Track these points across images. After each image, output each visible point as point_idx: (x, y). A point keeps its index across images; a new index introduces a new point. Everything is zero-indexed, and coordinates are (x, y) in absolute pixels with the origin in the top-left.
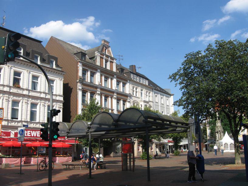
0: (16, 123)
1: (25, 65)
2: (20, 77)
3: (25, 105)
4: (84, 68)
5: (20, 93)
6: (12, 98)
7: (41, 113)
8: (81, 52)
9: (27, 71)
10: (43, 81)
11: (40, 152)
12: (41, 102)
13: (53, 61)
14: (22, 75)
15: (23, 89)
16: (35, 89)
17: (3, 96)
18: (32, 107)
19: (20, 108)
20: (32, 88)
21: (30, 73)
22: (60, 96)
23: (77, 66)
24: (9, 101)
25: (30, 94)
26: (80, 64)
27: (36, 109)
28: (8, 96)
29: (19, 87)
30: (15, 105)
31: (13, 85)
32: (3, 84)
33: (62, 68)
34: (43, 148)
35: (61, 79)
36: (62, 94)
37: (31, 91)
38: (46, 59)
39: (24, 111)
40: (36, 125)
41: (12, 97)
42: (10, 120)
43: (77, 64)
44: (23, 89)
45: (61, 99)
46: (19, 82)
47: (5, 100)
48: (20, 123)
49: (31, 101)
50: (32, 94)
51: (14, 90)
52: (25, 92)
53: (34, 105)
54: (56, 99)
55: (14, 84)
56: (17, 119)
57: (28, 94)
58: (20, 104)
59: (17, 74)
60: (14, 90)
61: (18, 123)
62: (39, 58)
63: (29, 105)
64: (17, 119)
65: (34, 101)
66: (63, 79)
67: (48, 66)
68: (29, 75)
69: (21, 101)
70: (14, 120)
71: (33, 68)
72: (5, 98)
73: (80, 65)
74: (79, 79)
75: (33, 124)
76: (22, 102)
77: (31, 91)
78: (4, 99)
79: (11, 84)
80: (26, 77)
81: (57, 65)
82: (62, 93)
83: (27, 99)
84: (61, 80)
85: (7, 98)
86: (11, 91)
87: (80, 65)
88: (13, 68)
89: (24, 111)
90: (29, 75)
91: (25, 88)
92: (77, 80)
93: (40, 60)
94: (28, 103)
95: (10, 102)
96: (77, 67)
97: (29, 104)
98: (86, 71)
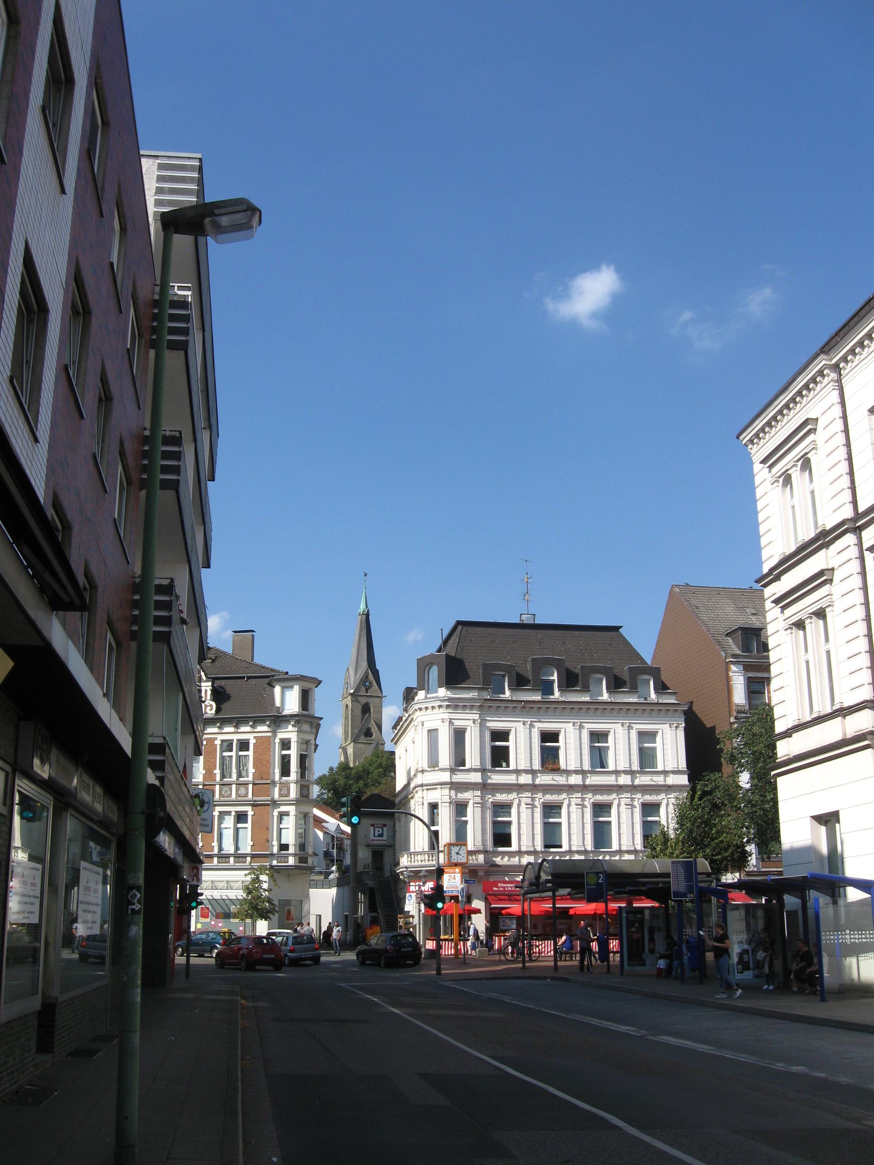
0: (506, 858)
1: (582, 711)
2: (557, 741)
3: (625, 812)
4: (751, 675)
5: (660, 783)
6: (541, 799)
7: (623, 826)
8: (740, 628)
9: (574, 725)
10: (621, 741)
11: (504, 926)
12: (619, 798)
13: (648, 681)
14: (561, 738)
15: (568, 772)
16: (603, 766)
17: (520, 795)
18: (495, 814)
19: (613, 818)
20: (593, 765)
21: (581, 727)
22: (675, 772)
23: (727, 674)
24: (633, 806)
25: (588, 782)
26: (733, 668)
27: (610, 817)
28: (529, 795)
29: (556, 770)
30: (552, 813)
31: (542, 767)
32: (515, 768)
33: (677, 693)
34: (510, 920)
35: (675, 725)
36: (685, 766)
37: (638, 772)
38: (528, 673)
39: (575, 828)
40: (509, 860)
41: (540, 795)
42: (542, 852)
43: (727, 670)
44: (568, 772)
45: (684, 780)
46: (556, 756)
47: (575, 806)
48: (517, 857)
49: (639, 799)
50: (592, 780)
51: (544, 779)
52: (575, 780)
53: (601, 809)
54: (618, 783)
55: (543, 762)
56: (560, 847)
57: (630, 783)
58: (614, 810)
59: (549, 737)
60: (544, 779)
61: (510, 857)
62: (652, 683)
63: (588, 812)
64: (560, 847)
65: (549, 798)
66: (683, 725)
67: (633, 699)
68: (629, 733)
69: (566, 802)
70: (552, 850)
71: (547, 712)
72: (524, 800)
73: (734, 672)
74: (735, 714)
75: (500, 857)
76: (619, 805)
77: (638, 772)
78: (622, 804)
79: (537, 765)
80: (572, 740)
81: (662, 688)
82: (683, 765)
83: (579, 795)
84: (677, 727)
85: (629, 801)
86: (637, 782)
87: (734, 672)
88: (587, 726)
89: (575, 828)
90: (629, 733)
91: (572, 767)
92: (730, 716)
93: (655, 689)
94: (583, 806)
95: (537, 807)
96: (728, 679)
97: (636, 807)
98: (764, 682)
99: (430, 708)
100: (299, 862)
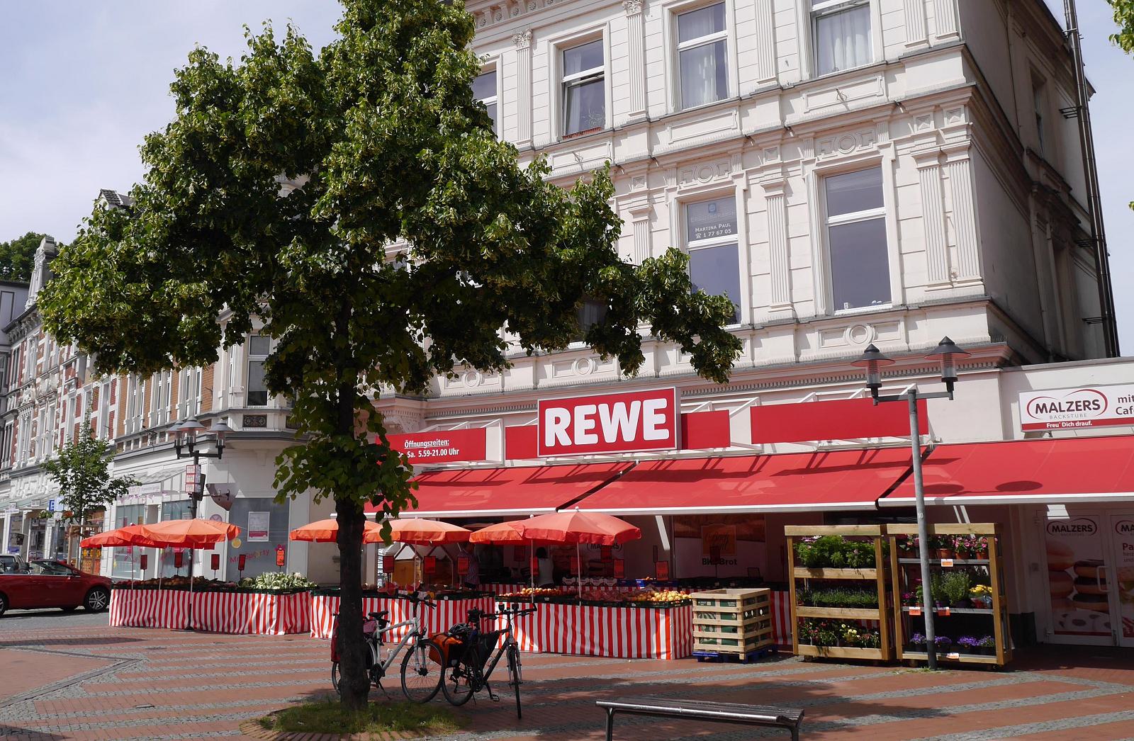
99: (488, 13)
100: (244, 426)
